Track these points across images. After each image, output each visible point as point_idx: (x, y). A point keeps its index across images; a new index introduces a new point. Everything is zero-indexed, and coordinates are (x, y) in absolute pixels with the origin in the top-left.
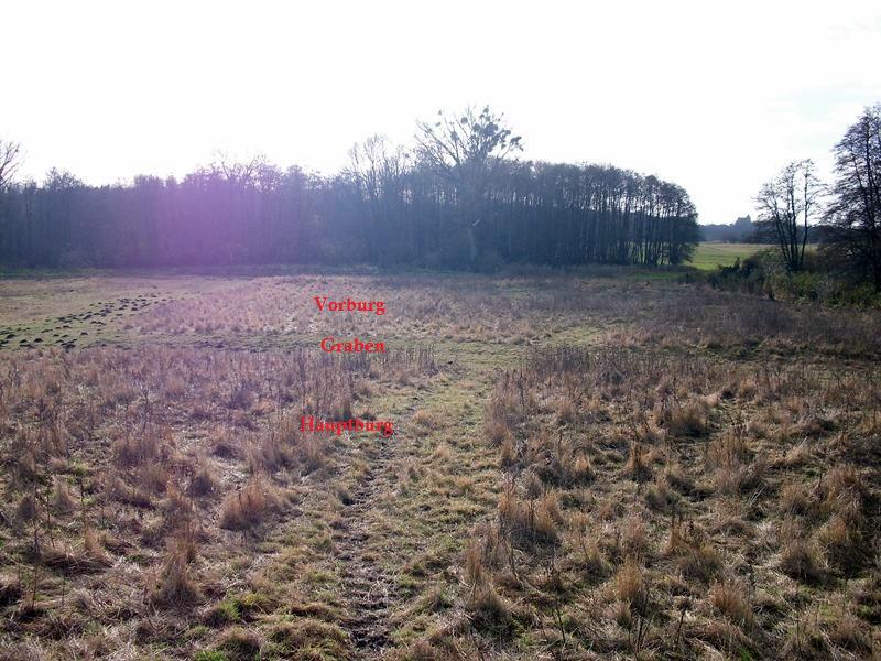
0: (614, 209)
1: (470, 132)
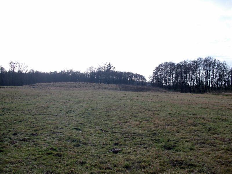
0: (202, 81)
1: (107, 67)
